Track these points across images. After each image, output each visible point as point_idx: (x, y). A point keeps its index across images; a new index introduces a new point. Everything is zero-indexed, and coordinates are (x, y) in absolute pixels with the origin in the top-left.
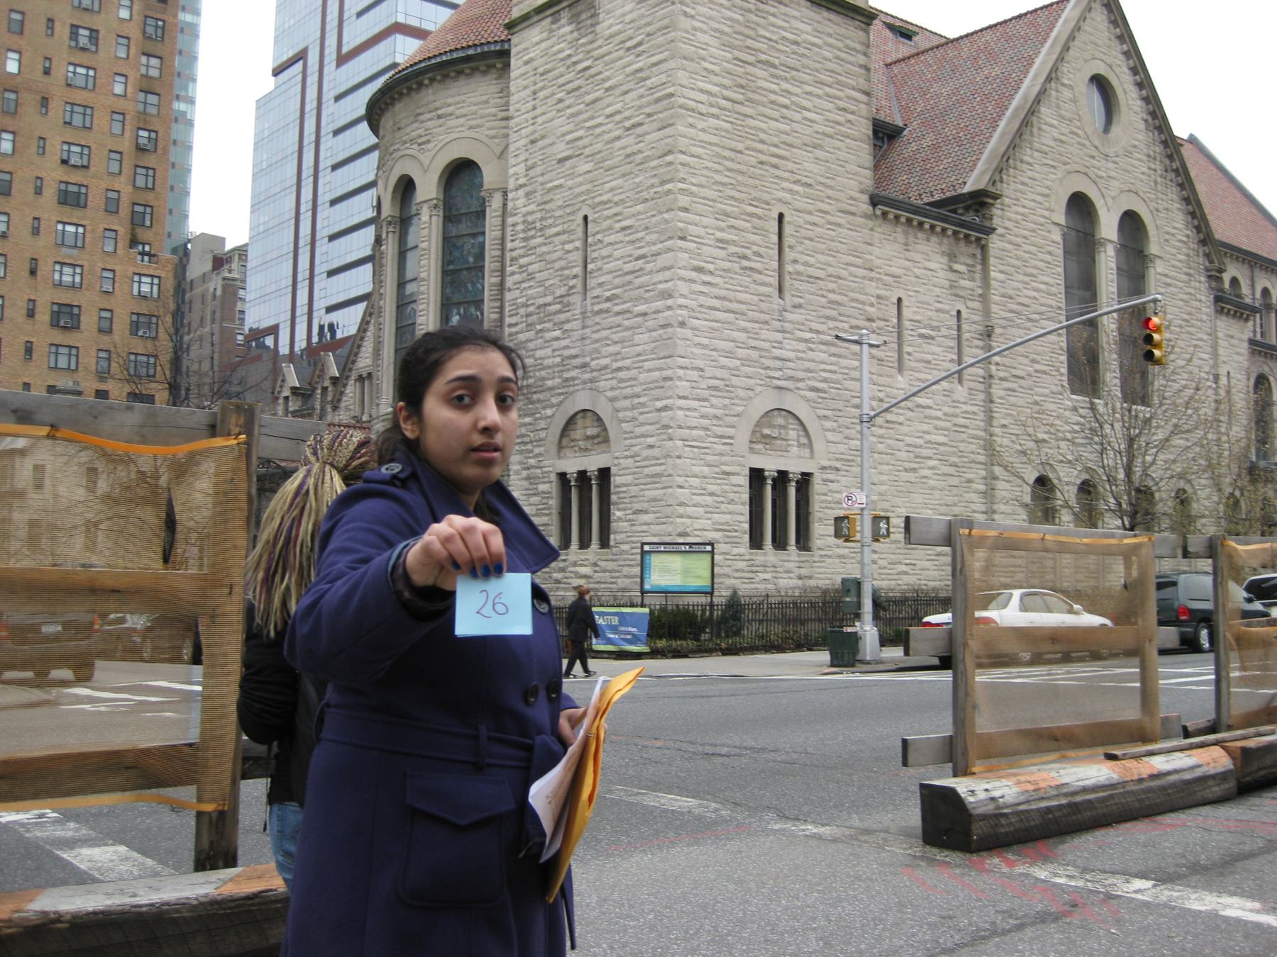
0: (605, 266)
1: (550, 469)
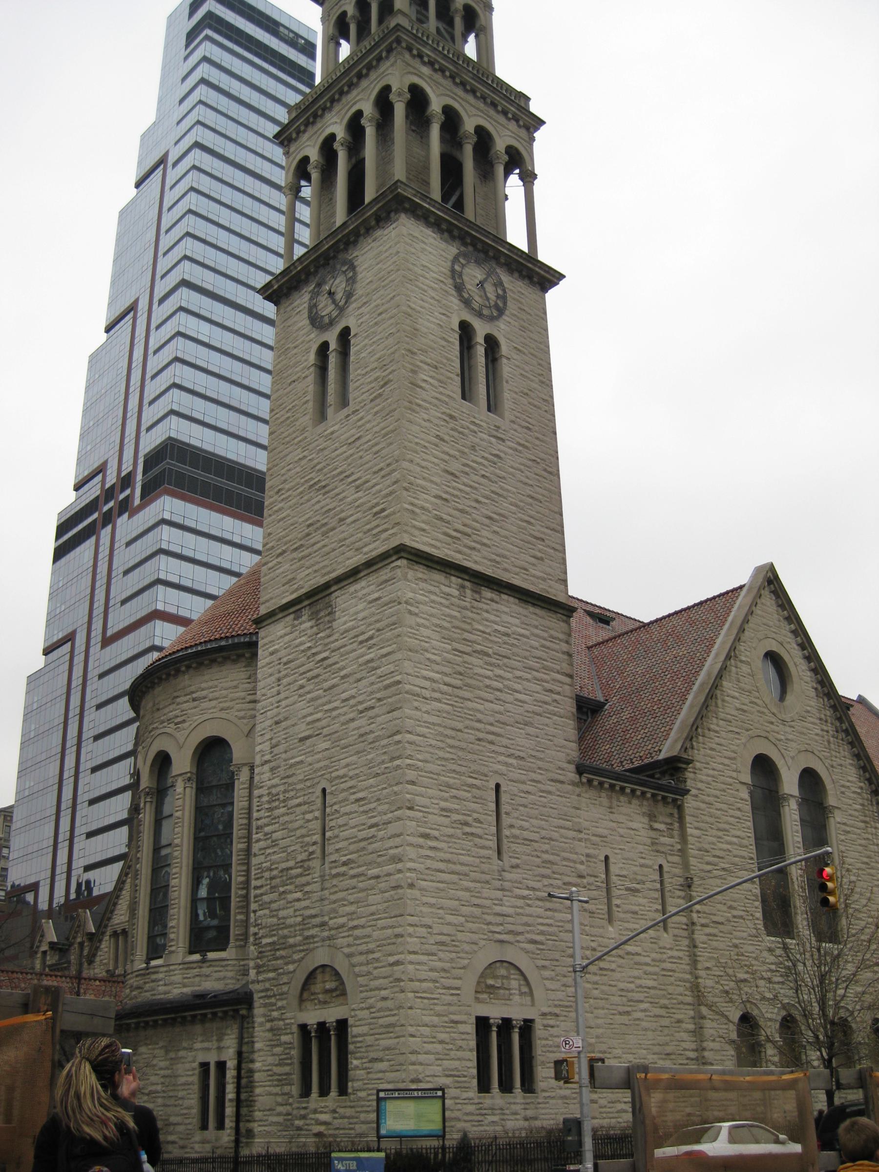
0: (341, 834)
1: (292, 1021)
